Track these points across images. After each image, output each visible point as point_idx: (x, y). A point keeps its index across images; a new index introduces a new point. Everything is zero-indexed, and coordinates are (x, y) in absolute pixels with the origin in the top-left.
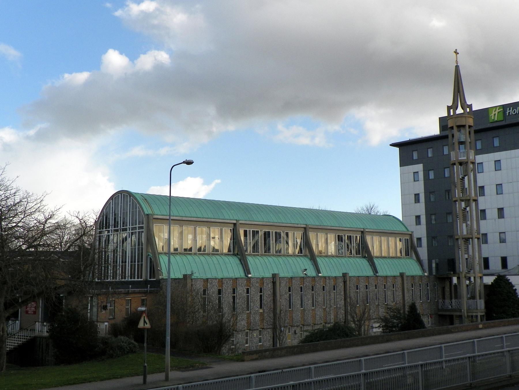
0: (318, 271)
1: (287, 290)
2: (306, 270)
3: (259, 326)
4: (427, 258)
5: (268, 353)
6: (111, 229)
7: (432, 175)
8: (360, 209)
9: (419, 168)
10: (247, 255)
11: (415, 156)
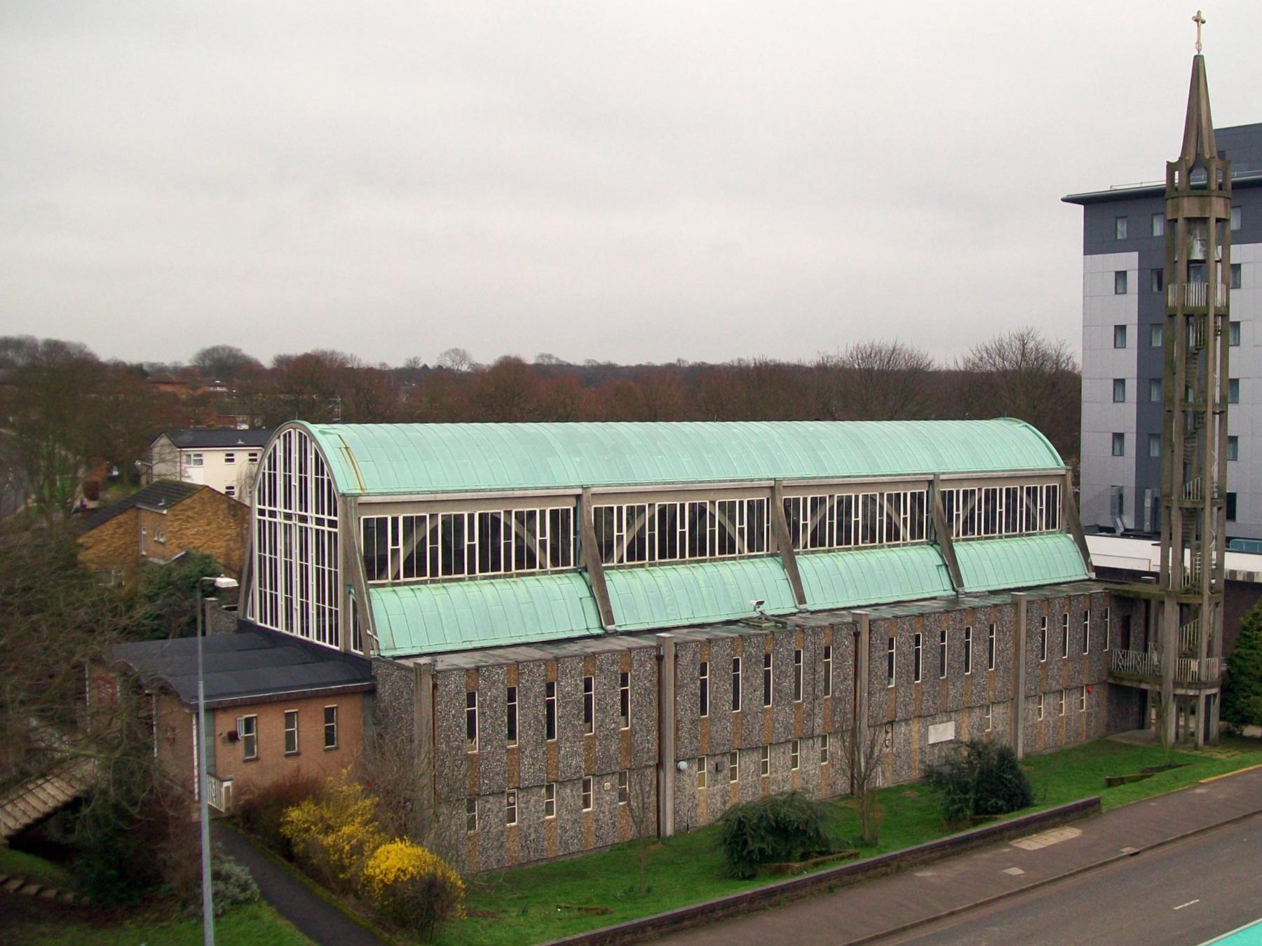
0: (801, 599)
2: (761, 603)
4: (1133, 485)
9: (1129, 261)
11: (1122, 230)
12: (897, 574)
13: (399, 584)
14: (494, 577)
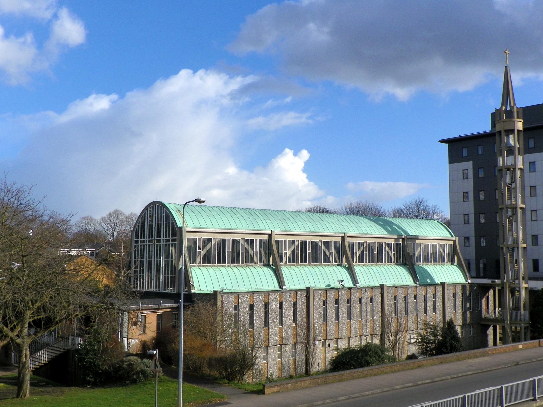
1: (322, 304)
2: (343, 281)
3: (291, 340)
4: (474, 258)
5: (290, 385)
6: (146, 239)
7: (481, 175)
8: (408, 203)
9: (469, 165)
10: (282, 265)
11: (465, 154)
12: (327, 276)
13: (200, 266)
14: (238, 266)
